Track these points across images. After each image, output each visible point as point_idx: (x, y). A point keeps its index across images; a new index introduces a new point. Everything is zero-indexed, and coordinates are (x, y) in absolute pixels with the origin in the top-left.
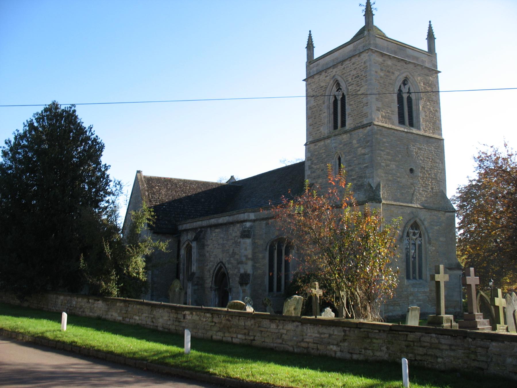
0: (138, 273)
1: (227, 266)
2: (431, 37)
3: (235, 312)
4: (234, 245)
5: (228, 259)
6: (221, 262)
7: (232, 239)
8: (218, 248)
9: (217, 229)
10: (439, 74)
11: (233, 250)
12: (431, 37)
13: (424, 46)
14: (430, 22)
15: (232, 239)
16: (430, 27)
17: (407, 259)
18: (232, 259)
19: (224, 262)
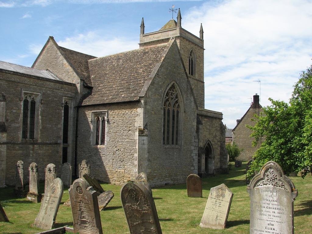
0: (257, 186)
1: (212, 143)
2: (202, 32)
3: (104, 110)
4: (216, 131)
5: (212, 139)
6: (209, 140)
7: (214, 127)
8: (206, 131)
9: (206, 119)
10: (204, 50)
11: (215, 134)
12: (202, 32)
13: (198, 35)
14: (201, 24)
15: (214, 127)
16: (202, 27)
17: (167, 113)
18: (215, 139)
19: (210, 141)
